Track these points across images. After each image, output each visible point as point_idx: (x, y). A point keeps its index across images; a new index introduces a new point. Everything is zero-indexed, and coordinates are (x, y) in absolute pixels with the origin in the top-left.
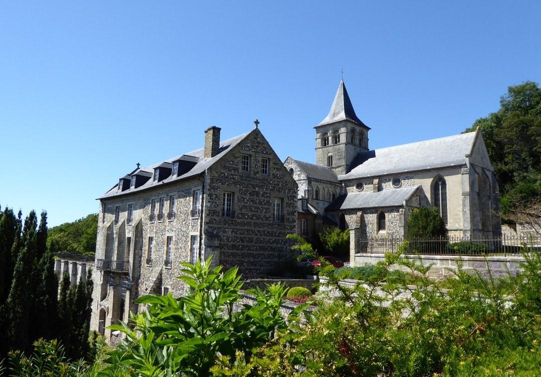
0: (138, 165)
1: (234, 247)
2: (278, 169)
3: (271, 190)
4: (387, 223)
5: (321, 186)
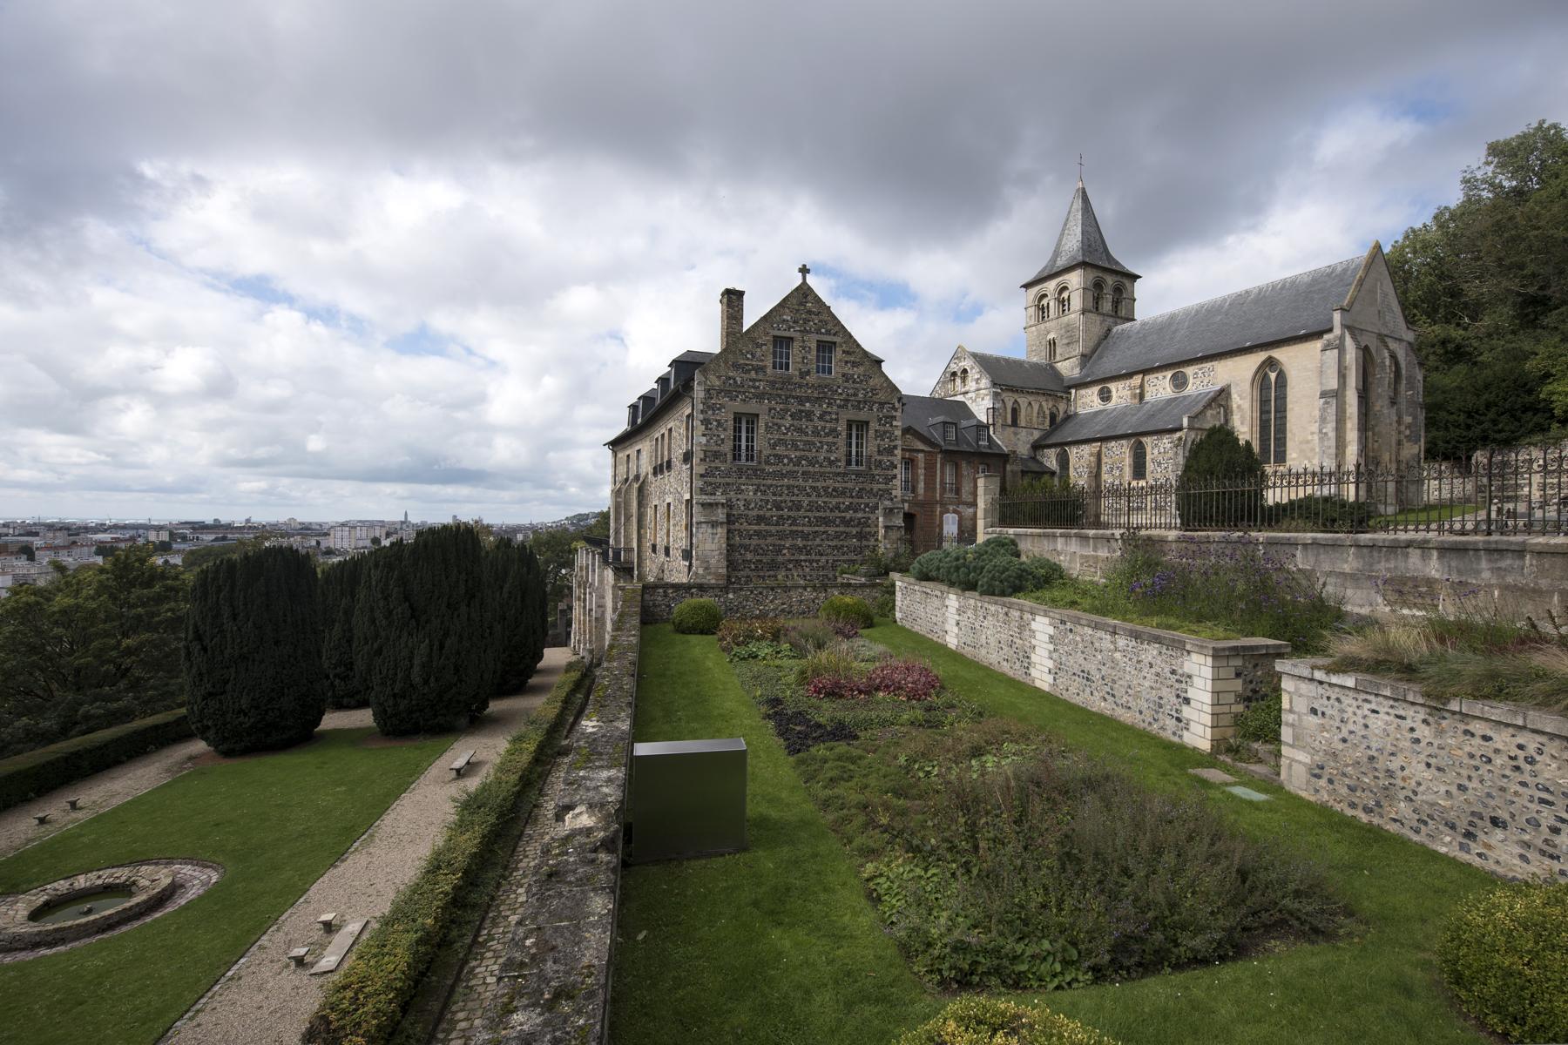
1: (760, 519)
2: (854, 364)
3: (839, 406)
4: (1150, 466)
5: (1023, 401)
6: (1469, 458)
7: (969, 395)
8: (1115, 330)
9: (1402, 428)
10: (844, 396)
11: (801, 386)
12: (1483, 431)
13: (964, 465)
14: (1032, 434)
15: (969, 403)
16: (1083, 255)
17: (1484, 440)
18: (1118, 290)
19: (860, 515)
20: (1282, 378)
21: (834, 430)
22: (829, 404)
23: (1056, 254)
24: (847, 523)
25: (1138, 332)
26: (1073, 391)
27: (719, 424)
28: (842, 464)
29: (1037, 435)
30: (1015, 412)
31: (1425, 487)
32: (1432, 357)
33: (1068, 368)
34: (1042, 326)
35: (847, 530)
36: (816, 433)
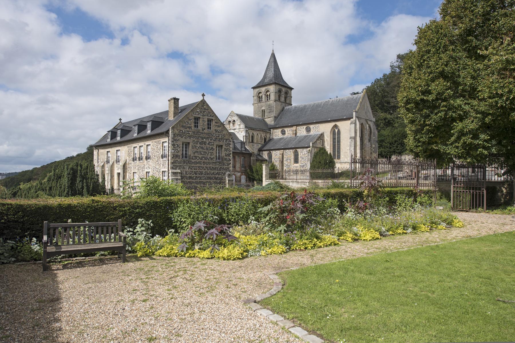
0: (120, 119)
1: (190, 178)
2: (218, 126)
3: (214, 140)
4: (300, 159)
5: (255, 133)
6: (390, 157)
7: (236, 130)
8: (285, 108)
9: (372, 148)
10: (215, 137)
11: (202, 134)
12: (394, 149)
13: (237, 157)
14: (258, 146)
15: (236, 133)
16: (275, 80)
17: (394, 152)
18: (286, 93)
19: (220, 176)
20: (339, 132)
21: (212, 148)
22: (211, 140)
23: (265, 77)
24: (216, 179)
25: (294, 110)
26: (272, 130)
27: (178, 146)
28: (215, 159)
29: (260, 146)
30: (253, 137)
31: (379, 167)
32: (382, 124)
33: (270, 121)
34: (260, 104)
35: (216, 181)
36: (207, 149)
